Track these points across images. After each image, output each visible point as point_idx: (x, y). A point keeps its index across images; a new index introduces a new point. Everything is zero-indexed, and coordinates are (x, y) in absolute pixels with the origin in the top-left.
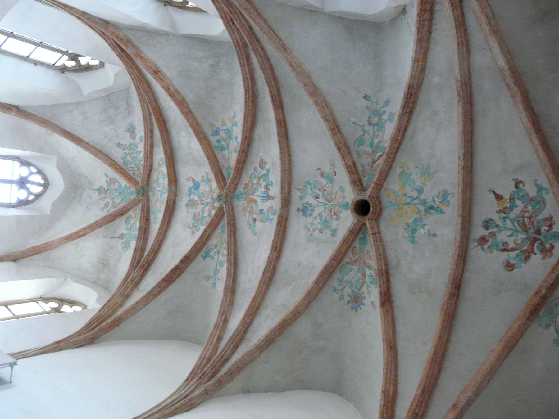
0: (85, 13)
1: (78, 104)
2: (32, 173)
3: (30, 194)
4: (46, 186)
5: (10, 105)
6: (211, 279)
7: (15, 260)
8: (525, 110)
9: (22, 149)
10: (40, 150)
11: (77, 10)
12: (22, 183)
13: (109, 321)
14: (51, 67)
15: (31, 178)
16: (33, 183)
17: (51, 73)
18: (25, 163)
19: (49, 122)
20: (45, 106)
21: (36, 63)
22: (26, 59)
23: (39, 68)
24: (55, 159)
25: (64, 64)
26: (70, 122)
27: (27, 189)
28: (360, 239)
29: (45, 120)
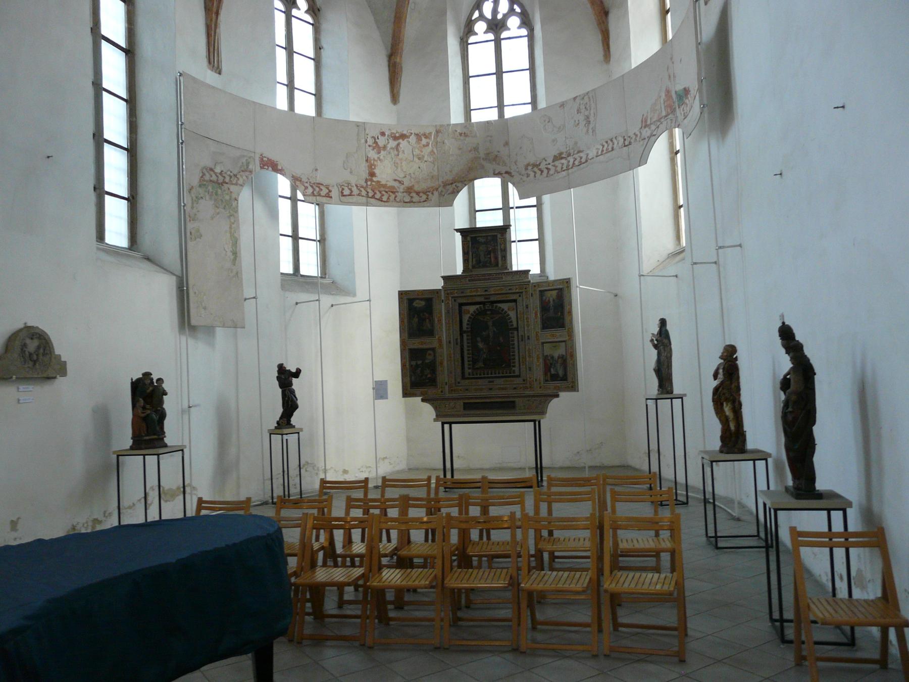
0: (205, 8)
2: (482, 17)
3: (511, 11)
5: (389, 66)
6: (195, 182)
7: (606, 13)
9: (445, 38)
10: (443, 13)
11: (206, 19)
12: (496, 26)
13: (497, 643)
15: (488, 14)
16: (495, 11)
17: (325, 26)
18: (469, 30)
19: (396, 13)
20: (376, 21)
21: (318, 47)
22: (317, 61)
23: (324, 43)
25: (306, 12)
27: (506, 16)
29: (395, 17)
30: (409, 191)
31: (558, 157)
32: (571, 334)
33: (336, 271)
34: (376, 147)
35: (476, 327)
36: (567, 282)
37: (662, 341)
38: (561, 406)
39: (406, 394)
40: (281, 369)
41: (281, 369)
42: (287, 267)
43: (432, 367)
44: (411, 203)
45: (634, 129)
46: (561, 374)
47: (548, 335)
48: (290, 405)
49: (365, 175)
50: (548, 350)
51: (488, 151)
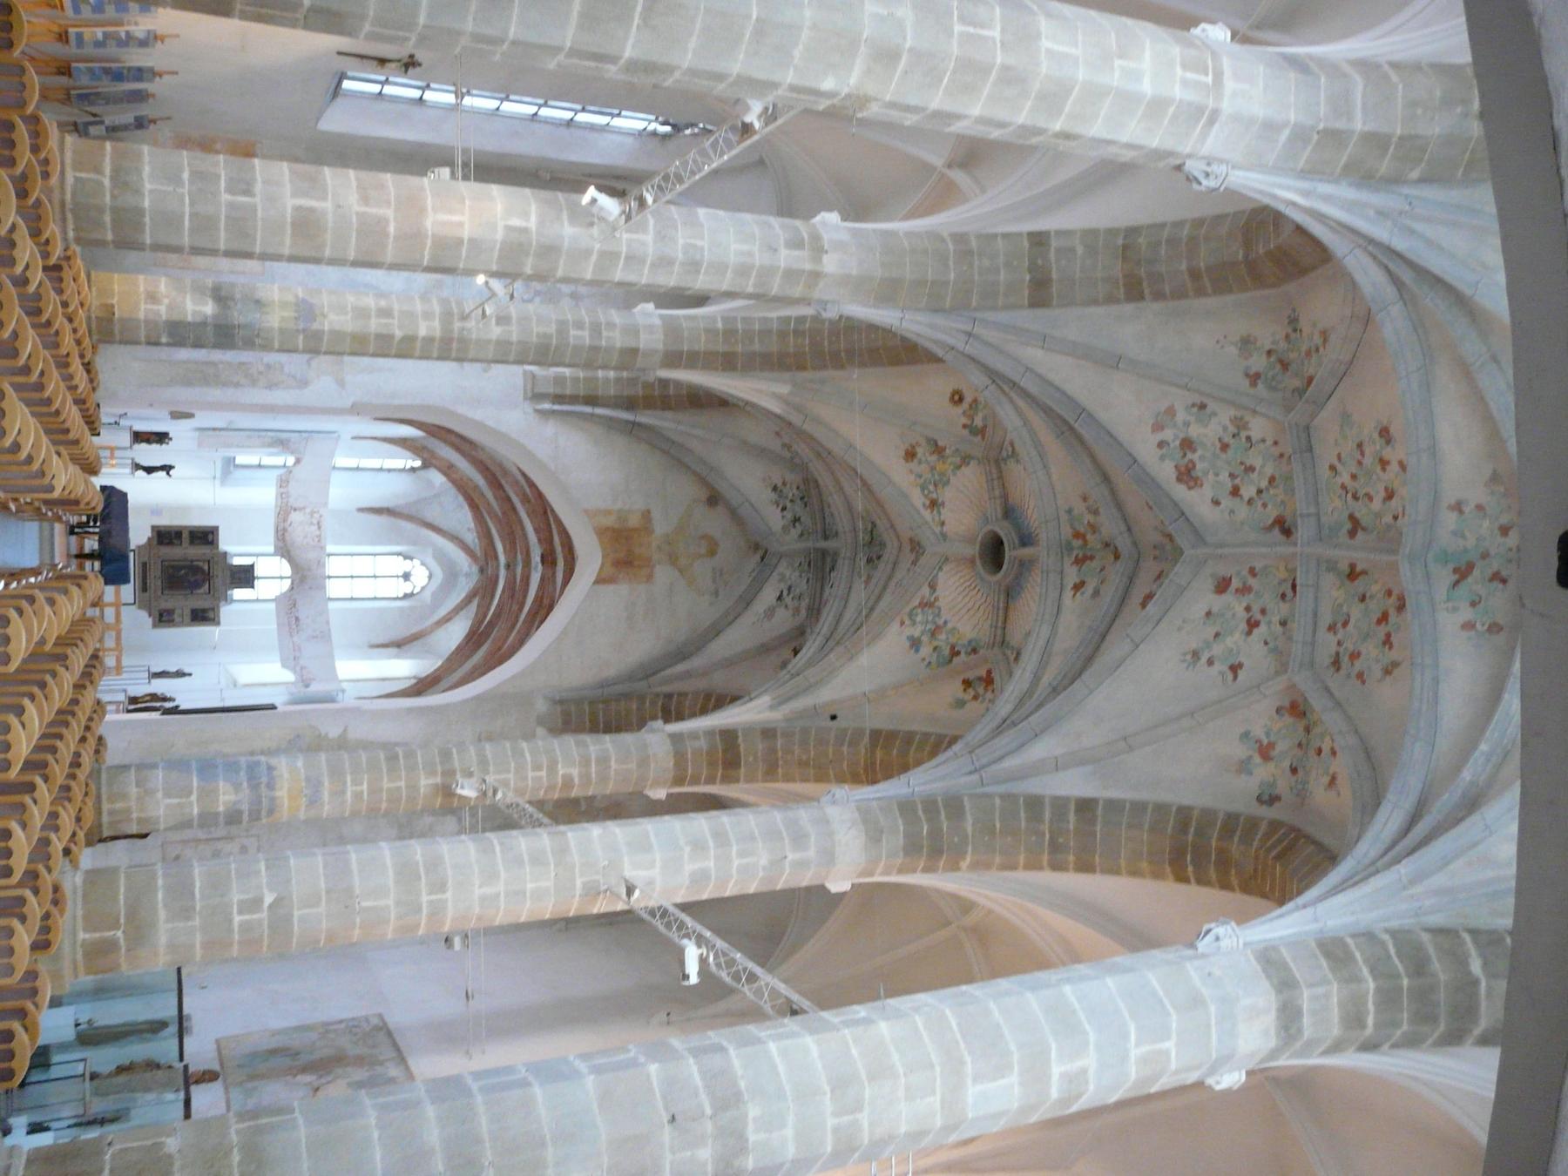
1: (435, 496)
4: (430, 577)
8: (982, 544)
10: (415, 543)
12: (406, 576)
14: (403, 470)
17: (404, 475)
18: (407, 557)
21: (389, 470)
22: (358, 469)
23: (392, 474)
24: (430, 551)
26: (432, 514)
28: (619, 58)
30: (285, 530)
31: (297, 619)
32: (188, 625)
33: (239, 473)
34: (312, 513)
35: (196, 570)
36: (218, 624)
37: (180, 674)
38: (144, 618)
39: (153, 528)
40: (171, 467)
41: (171, 467)
42: (240, 460)
43: (170, 543)
44: (277, 531)
45: (302, 662)
46: (164, 618)
47: (187, 612)
48: (149, 470)
49: (296, 505)
50: (178, 612)
51: (306, 578)
